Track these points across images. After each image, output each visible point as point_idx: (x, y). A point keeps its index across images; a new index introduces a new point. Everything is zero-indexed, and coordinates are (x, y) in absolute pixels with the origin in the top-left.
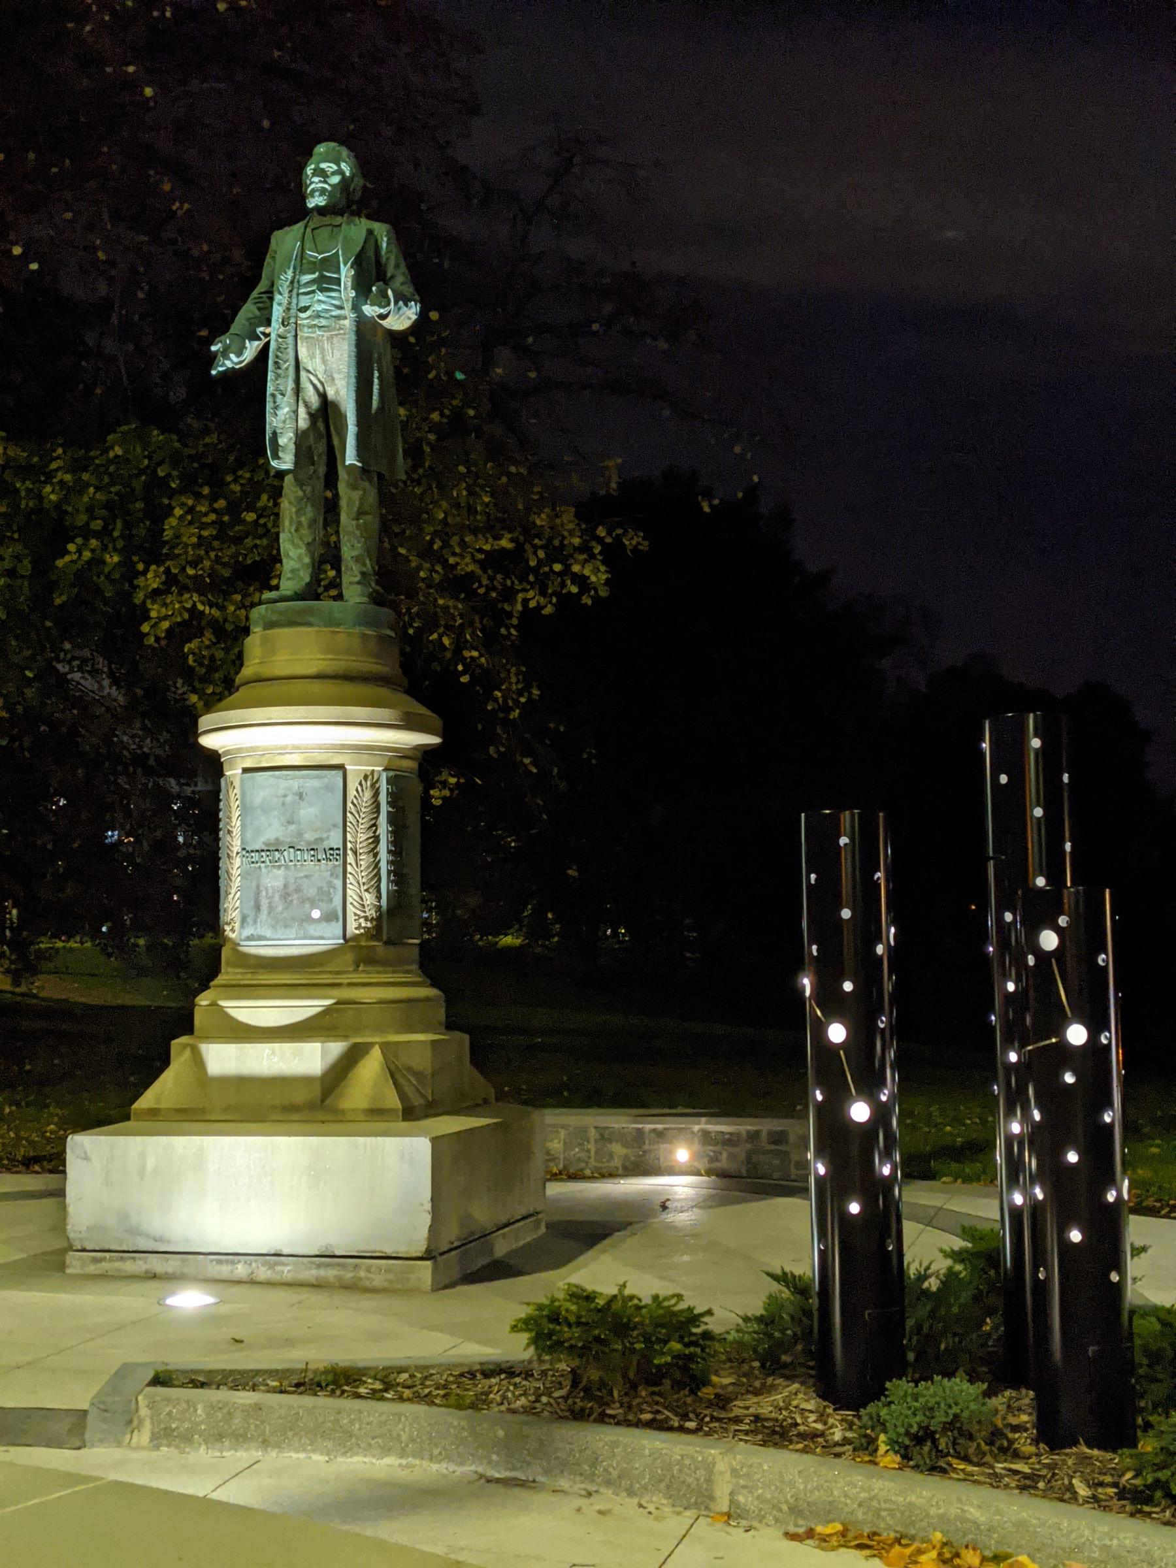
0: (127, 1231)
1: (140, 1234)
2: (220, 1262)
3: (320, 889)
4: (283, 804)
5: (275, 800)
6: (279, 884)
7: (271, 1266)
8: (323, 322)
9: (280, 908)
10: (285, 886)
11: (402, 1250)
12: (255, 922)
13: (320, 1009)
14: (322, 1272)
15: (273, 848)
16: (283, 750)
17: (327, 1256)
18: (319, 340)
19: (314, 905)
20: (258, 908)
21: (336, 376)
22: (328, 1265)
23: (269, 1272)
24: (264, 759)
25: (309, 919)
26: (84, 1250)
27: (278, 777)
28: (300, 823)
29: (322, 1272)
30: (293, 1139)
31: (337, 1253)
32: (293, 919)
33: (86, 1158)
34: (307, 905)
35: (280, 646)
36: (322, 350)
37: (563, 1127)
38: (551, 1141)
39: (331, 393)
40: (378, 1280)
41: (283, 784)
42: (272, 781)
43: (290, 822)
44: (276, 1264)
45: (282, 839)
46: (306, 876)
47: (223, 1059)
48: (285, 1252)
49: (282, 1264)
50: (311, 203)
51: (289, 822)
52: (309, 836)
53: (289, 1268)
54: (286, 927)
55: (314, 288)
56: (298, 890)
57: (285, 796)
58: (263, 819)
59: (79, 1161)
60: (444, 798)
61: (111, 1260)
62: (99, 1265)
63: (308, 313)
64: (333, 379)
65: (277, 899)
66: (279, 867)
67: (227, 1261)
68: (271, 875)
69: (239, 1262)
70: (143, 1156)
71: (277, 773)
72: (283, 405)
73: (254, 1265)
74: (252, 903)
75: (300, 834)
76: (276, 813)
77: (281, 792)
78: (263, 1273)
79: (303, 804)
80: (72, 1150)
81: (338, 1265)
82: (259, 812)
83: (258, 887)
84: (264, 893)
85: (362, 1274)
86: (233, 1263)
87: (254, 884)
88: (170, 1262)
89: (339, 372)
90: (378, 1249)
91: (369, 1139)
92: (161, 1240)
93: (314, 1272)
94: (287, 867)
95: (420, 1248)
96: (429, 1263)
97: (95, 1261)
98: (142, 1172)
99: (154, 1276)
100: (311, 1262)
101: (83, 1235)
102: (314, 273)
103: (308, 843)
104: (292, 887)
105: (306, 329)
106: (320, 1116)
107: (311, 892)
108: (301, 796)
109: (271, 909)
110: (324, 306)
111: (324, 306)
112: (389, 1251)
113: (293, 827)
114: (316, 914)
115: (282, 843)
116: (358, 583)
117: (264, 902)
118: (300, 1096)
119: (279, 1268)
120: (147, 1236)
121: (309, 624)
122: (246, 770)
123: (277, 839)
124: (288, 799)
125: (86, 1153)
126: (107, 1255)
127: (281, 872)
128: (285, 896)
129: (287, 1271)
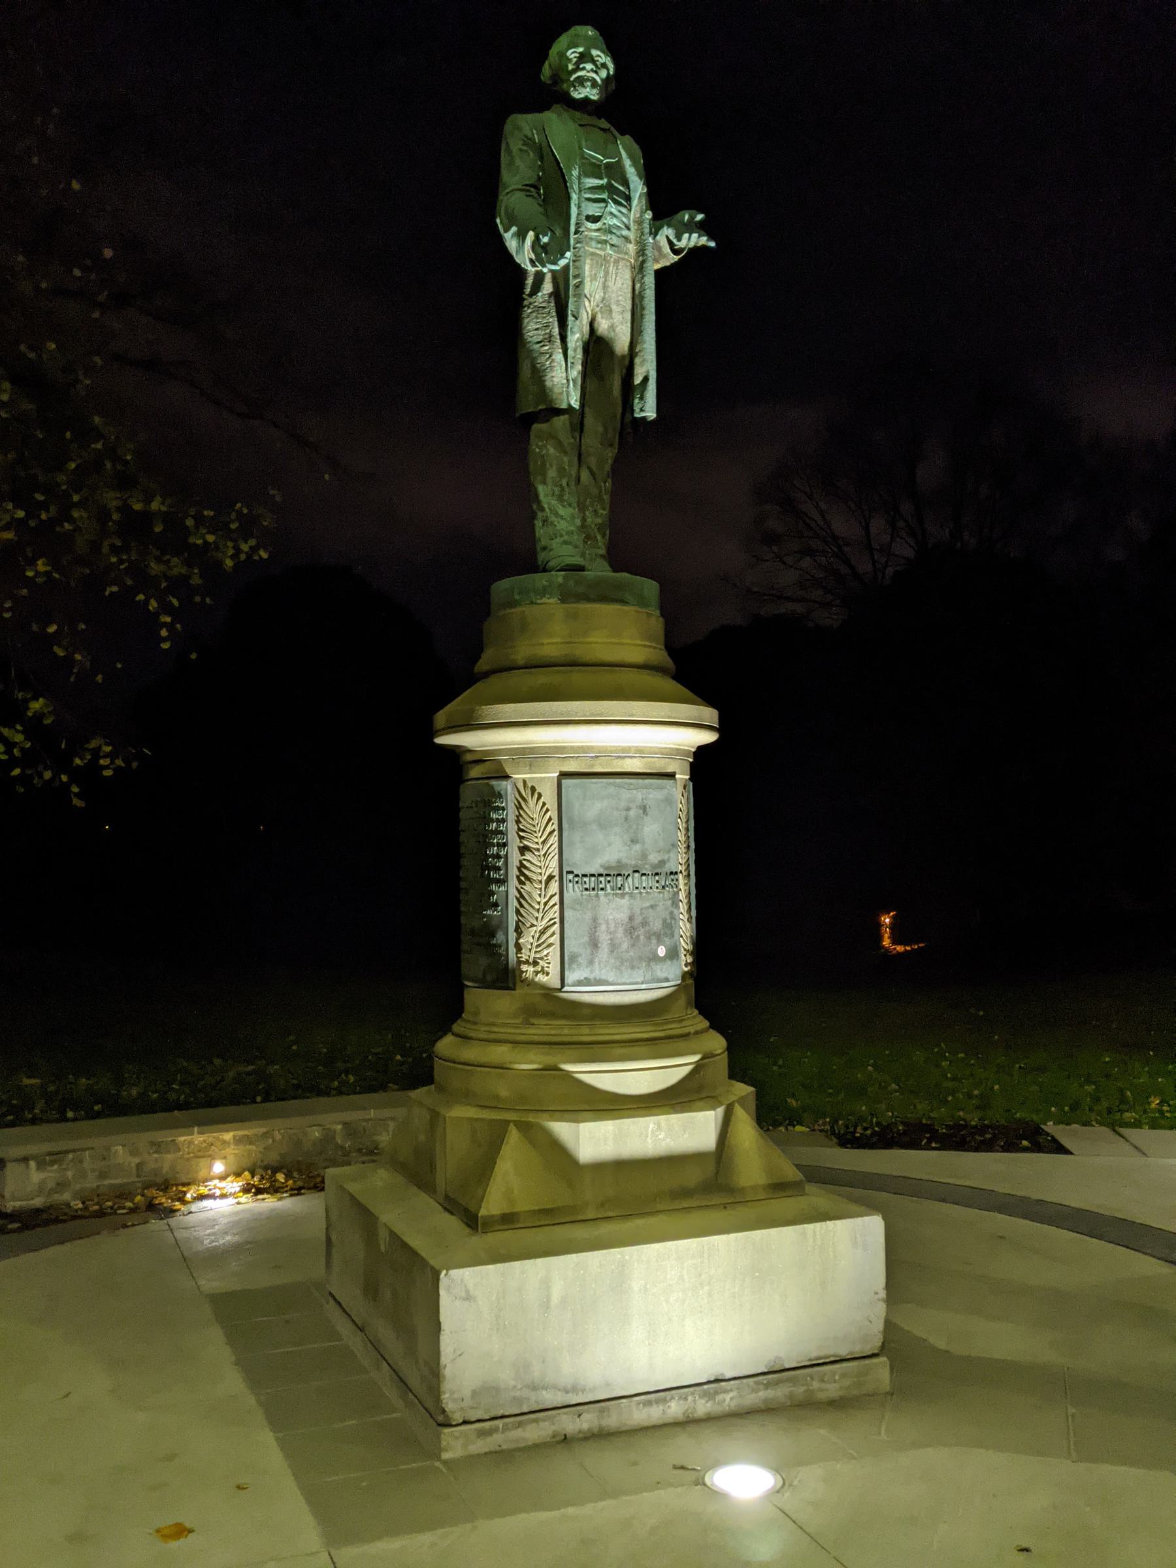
0: (528, 1387)
1: (545, 1388)
2: (649, 1403)
3: (664, 921)
4: (626, 819)
5: (615, 813)
6: (623, 916)
7: (710, 1396)
8: (615, 240)
9: (625, 946)
10: (631, 918)
11: (858, 1350)
12: (591, 962)
13: (690, 1067)
14: (770, 1393)
15: (614, 875)
16: (624, 753)
17: (776, 1373)
18: (605, 259)
19: (660, 942)
20: (594, 944)
21: (614, 307)
22: (777, 1383)
23: (709, 1405)
24: (598, 761)
25: (655, 958)
26: (465, 1422)
27: (620, 786)
28: (644, 843)
29: (770, 1393)
30: (732, 1236)
31: (787, 1366)
32: (640, 959)
33: (468, 1298)
34: (654, 941)
35: (546, 623)
36: (607, 273)
37: (392, 1119)
38: (380, 1134)
39: (603, 326)
40: (832, 1390)
41: (625, 795)
42: (612, 790)
43: (634, 841)
44: (716, 1393)
45: (625, 861)
46: (652, 907)
47: (593, 1140)
48: (728, 1375)
49: (726, 1391)
50: (578, 94)
51: (632, 841)
52: (654, 858)
53: (731, 1395)
54: (633, 968)
55: (604, 196)
56: (645, 923)
57: (628, 809)
58: (601, 836)
59: (458, 1303)
60: (117, 770)
61: (506, 1428)
62: (489, 1439)
63: (598, 225)
64: (611, 311)
65: (620, 934)
66: (623, 896)
67: (657, 1402)
68: (612, 905)
69: (672, 1398)
70: (546, 1284)
71: (618, 781)
72: (575, 329)
73: (690, 1398)
74: (586, 939)
75: (644, 856)
76: (617, 829)
77: (623, 804)
78: (703, 1407)
79: (647, 819)
80: (448, 1289)
81: (788, 1380)
82: (594, 827)
83: (595, 920)
84: (603, 927)
85: (816, 1385)
86: (664, 1401)
87: (588, 916)
88: (585, 1416)
89: (618, 303)
90: (831, 1352)
91: (818, 1225)
92: (575, 1389)
93: (762, 1394)
94: (631, 895)
95: (875, 1344)
96: (883, 1359)
97: (482, 1434)
98: (546, 1305)
99: (566, 1440)
100: (756, 1383)
101: (465, 1404)
102: (601, 179)
103: (654, 866)
104: (638, 920)
105: (593, 244)
106: (717, 1200)
107: (657, 925)
108: (644, 809)
109: (613, 947)
110: (615, 221)
111: (615, 221)
112: (843, 1352)
113: (638, 847)
114: (662, 951)
115: (625, 866)
116: (602, 556)
117: (604, 938)
118: (693, 1176)
119: (719, 1397)
120: (555, 1387)
121: (622, 601)
122: (564, 775)
123: (619, 862)
124: (632, 813)
125: (467, 1292)
126: (499, 1423)
127: (625, 902)
128: (631, 930)
129: (729, 1400)
